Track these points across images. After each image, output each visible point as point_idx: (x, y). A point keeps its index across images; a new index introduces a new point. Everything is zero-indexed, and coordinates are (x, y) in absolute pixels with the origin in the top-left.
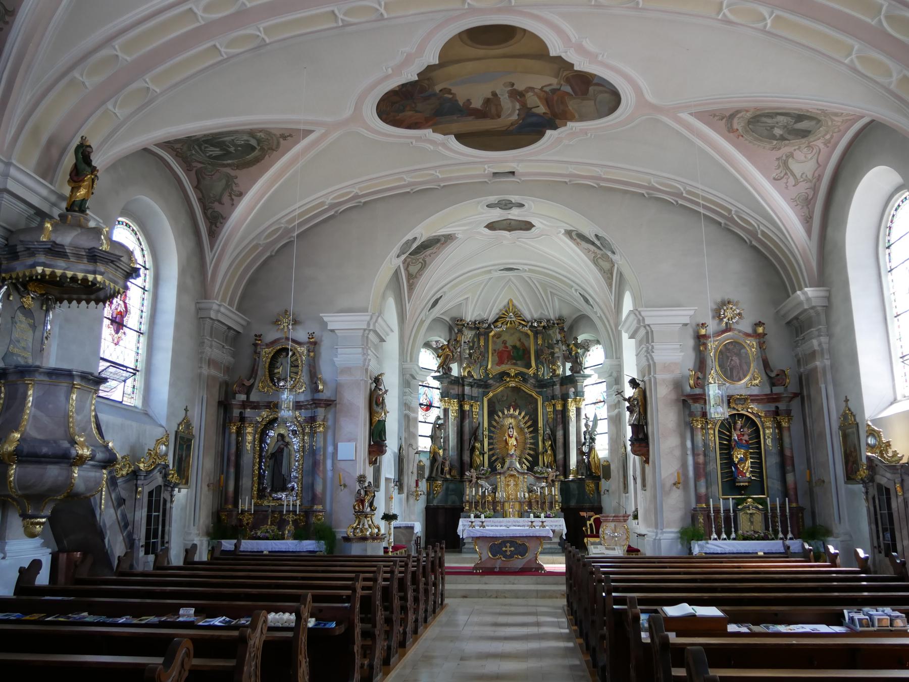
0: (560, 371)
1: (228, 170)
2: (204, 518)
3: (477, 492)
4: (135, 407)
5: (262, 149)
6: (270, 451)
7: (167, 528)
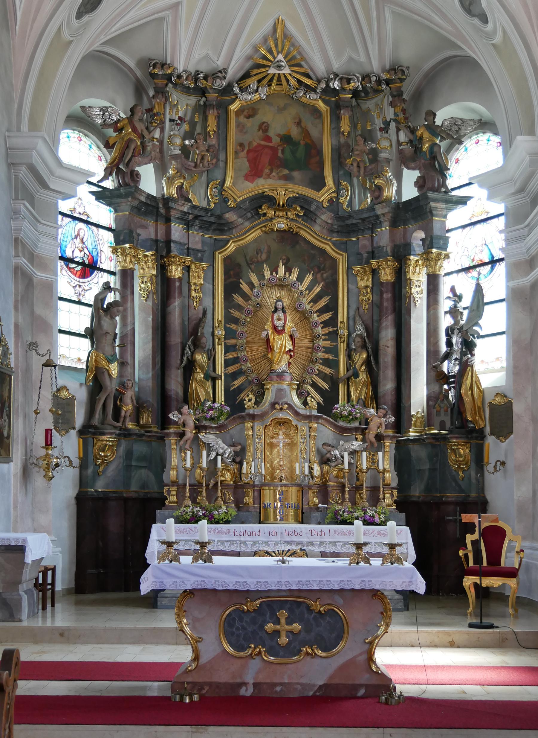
0: (391, 193)
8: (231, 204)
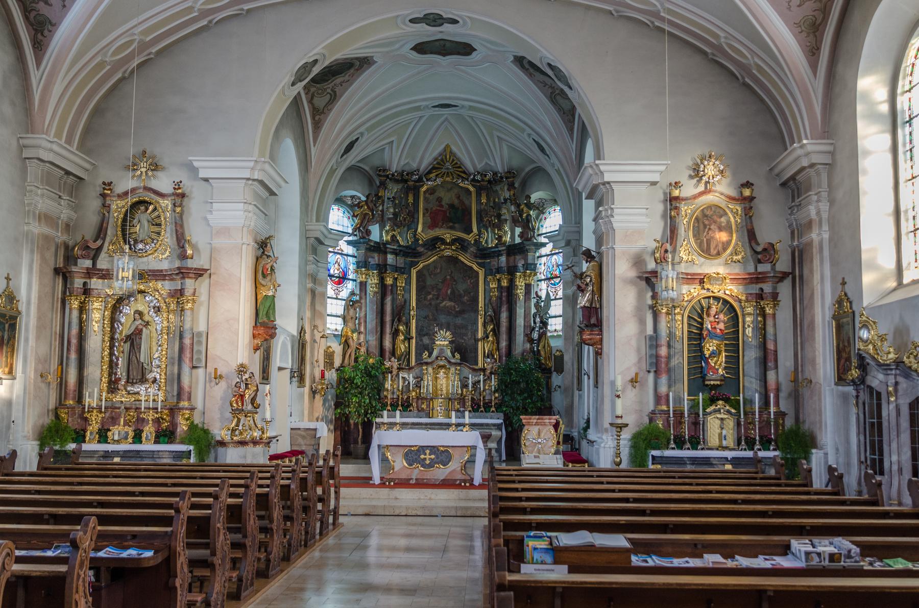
0: (507, 238)
8: (420, 242)
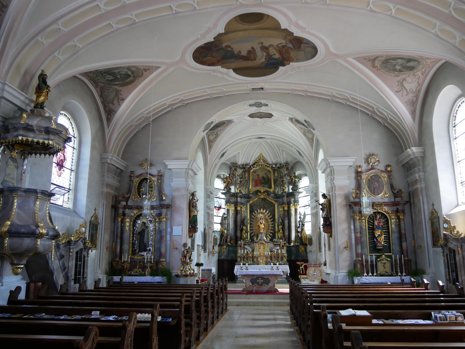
0: (286, 190)
1: (117, 87)
2: (104, 265)
3: (244, 252)
4: (69, 208)
5: (134, 76)
6: (138, 231)
7: (85, 270)
